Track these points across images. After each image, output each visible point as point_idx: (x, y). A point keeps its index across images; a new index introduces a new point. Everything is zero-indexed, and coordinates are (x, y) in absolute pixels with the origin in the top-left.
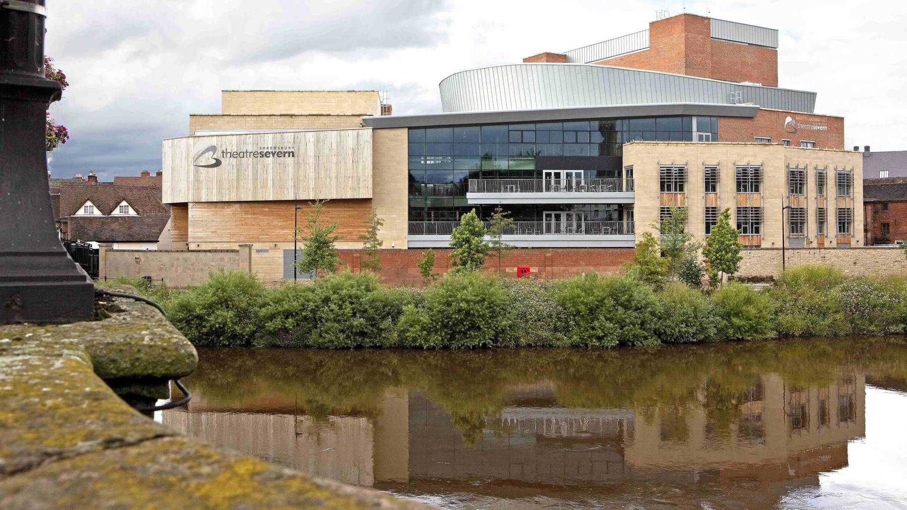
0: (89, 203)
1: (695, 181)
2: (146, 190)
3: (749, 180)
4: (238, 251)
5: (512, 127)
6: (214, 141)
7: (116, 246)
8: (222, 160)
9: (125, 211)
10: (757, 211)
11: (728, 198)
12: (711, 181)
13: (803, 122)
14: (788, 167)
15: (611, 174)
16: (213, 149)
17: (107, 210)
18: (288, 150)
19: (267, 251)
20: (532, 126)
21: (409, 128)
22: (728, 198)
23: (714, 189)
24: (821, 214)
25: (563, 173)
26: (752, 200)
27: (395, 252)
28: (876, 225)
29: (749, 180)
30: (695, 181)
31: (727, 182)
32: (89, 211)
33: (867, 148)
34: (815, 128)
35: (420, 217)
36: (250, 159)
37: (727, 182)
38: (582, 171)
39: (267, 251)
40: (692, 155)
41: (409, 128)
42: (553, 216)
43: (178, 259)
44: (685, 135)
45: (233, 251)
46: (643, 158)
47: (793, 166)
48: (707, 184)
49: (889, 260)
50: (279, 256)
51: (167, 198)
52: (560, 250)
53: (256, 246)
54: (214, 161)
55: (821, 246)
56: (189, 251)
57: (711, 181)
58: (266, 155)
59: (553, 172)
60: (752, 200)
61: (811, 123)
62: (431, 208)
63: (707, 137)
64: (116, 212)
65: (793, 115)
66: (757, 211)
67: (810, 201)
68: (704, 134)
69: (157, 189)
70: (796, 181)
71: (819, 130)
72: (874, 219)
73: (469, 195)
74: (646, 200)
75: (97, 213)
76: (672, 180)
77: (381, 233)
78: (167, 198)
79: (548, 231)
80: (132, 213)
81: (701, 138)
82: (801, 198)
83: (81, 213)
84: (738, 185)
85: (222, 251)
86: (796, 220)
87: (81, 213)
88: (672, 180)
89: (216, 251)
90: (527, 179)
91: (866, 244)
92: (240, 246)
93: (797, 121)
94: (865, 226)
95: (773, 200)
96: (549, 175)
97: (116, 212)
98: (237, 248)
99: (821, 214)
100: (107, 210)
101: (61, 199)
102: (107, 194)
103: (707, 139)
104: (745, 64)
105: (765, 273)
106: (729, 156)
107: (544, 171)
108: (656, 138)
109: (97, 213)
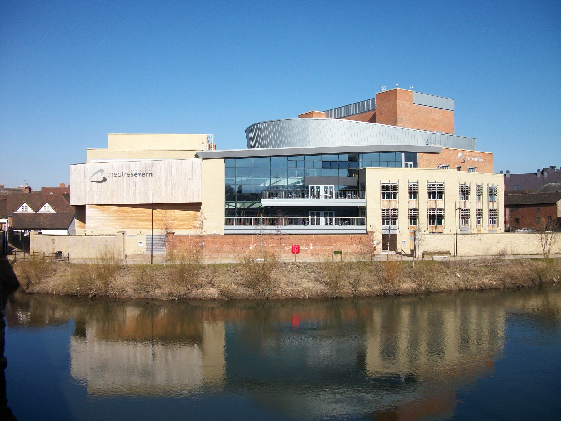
0: (25, 205)
1: (403, 192)
2: (60, 196)
3: (436, 192)
4: (116, 236)
5: (290, 158)
6: (102, 166)
7: (44, 232)
8: (107, 178)
9: (47, 209)
10: (441, 211)
11: (423, 204)
12: (413, 193)
13: (469, 156)
14: (488, 185)
15: (356, 188)
16: (101, 171)
17: (36, 208)
18: (149, 172)
19: (135, 235)
20: (302, 157)
21: (225, 158)
22: (423, 204)
23: (414, 198)
24: (480, 212)
25: (322, 187)
26: (438, 204)
27: (215, 237)
28: (512, 219)
29: (436, 192)
30: (403, 192)
31: (423, 193)
32: (25, 209)
33: (508, 172)
34: (476, 160)
35: (232, 216)
36: (125, 177)
37: (423, 193)
38: (334, 186)
39: (135, 235)
40: (401, 176)
41: (225, 158)
42: (316, 214)
43: (79, 240)
44: (396, 164)
45: (113, 235)
46: (375, 177)
47: (490, 185)
48: (411, 194)
49: (527, 244)
50: (143, 239)
51: (74, 201)
52: (319, 235)
53: (128, 232)
54: (103, 179)
55: (479, 233)
56: (86, 235)
57: (413, 193)
58: (135, 175)
59: (315, 186)
60: (438, 204)
61: (473, 157)
62: (243, 207)
63: (411, 165)
64: (42, 210)
65: (463, 152)
66: (441, 211)
67: (472, 204)
68: (409, 163)
69: (67, 196)
70: (465, 192)
71: (478, 162)
72: (511, 215)
73: (262, 200)
74: (373, 203)
75: (30, 211)
76: (389, 192)
77: (205, 225)
78: (74, 201)
79: (313, 223)
80: (51, 210)
81: (407, 166)
82: (468, 203)
83: (20, 211)
84: (430, 194)
85: (106, 235)
86: (465, 216)
87: (20, 211)
88: (389, 192)
89: (103, 235)
90: (302, 191)
91: (507, 230)
92: (118, 232)
93: (466, 155)
94: (505, 219)
95: (450, 203)
96: (313, 188)
97: (42, 210)
98: (116, 234)
99: (480, 212)
100: (36, 208)
101: (8, 201)
102: (36, 198)
103: (411, 166)
104: (434, 120)
105: (445, 249)
106: (424, 176)
107: (310, 186)
108: (388, 166)
109: (30, 211)
